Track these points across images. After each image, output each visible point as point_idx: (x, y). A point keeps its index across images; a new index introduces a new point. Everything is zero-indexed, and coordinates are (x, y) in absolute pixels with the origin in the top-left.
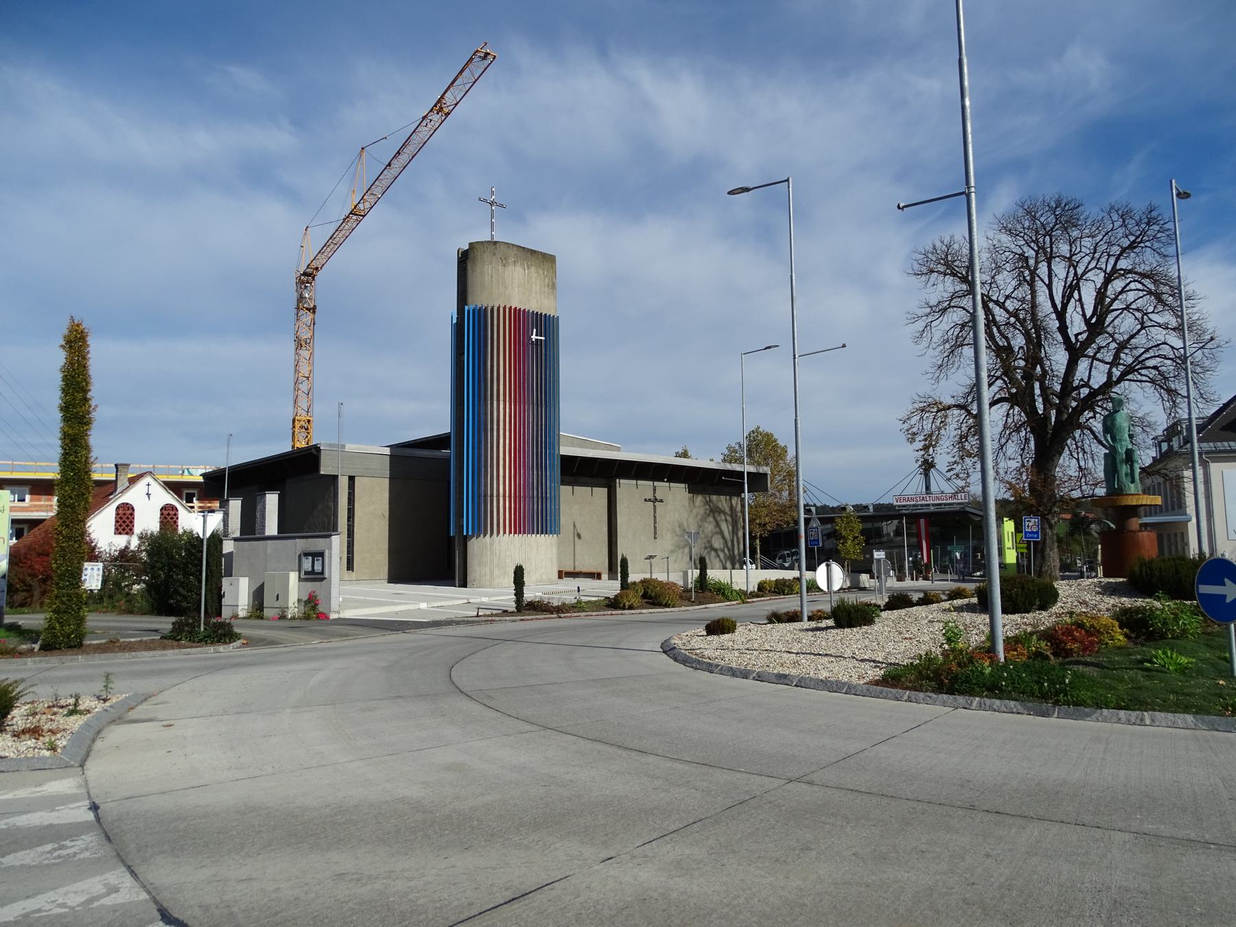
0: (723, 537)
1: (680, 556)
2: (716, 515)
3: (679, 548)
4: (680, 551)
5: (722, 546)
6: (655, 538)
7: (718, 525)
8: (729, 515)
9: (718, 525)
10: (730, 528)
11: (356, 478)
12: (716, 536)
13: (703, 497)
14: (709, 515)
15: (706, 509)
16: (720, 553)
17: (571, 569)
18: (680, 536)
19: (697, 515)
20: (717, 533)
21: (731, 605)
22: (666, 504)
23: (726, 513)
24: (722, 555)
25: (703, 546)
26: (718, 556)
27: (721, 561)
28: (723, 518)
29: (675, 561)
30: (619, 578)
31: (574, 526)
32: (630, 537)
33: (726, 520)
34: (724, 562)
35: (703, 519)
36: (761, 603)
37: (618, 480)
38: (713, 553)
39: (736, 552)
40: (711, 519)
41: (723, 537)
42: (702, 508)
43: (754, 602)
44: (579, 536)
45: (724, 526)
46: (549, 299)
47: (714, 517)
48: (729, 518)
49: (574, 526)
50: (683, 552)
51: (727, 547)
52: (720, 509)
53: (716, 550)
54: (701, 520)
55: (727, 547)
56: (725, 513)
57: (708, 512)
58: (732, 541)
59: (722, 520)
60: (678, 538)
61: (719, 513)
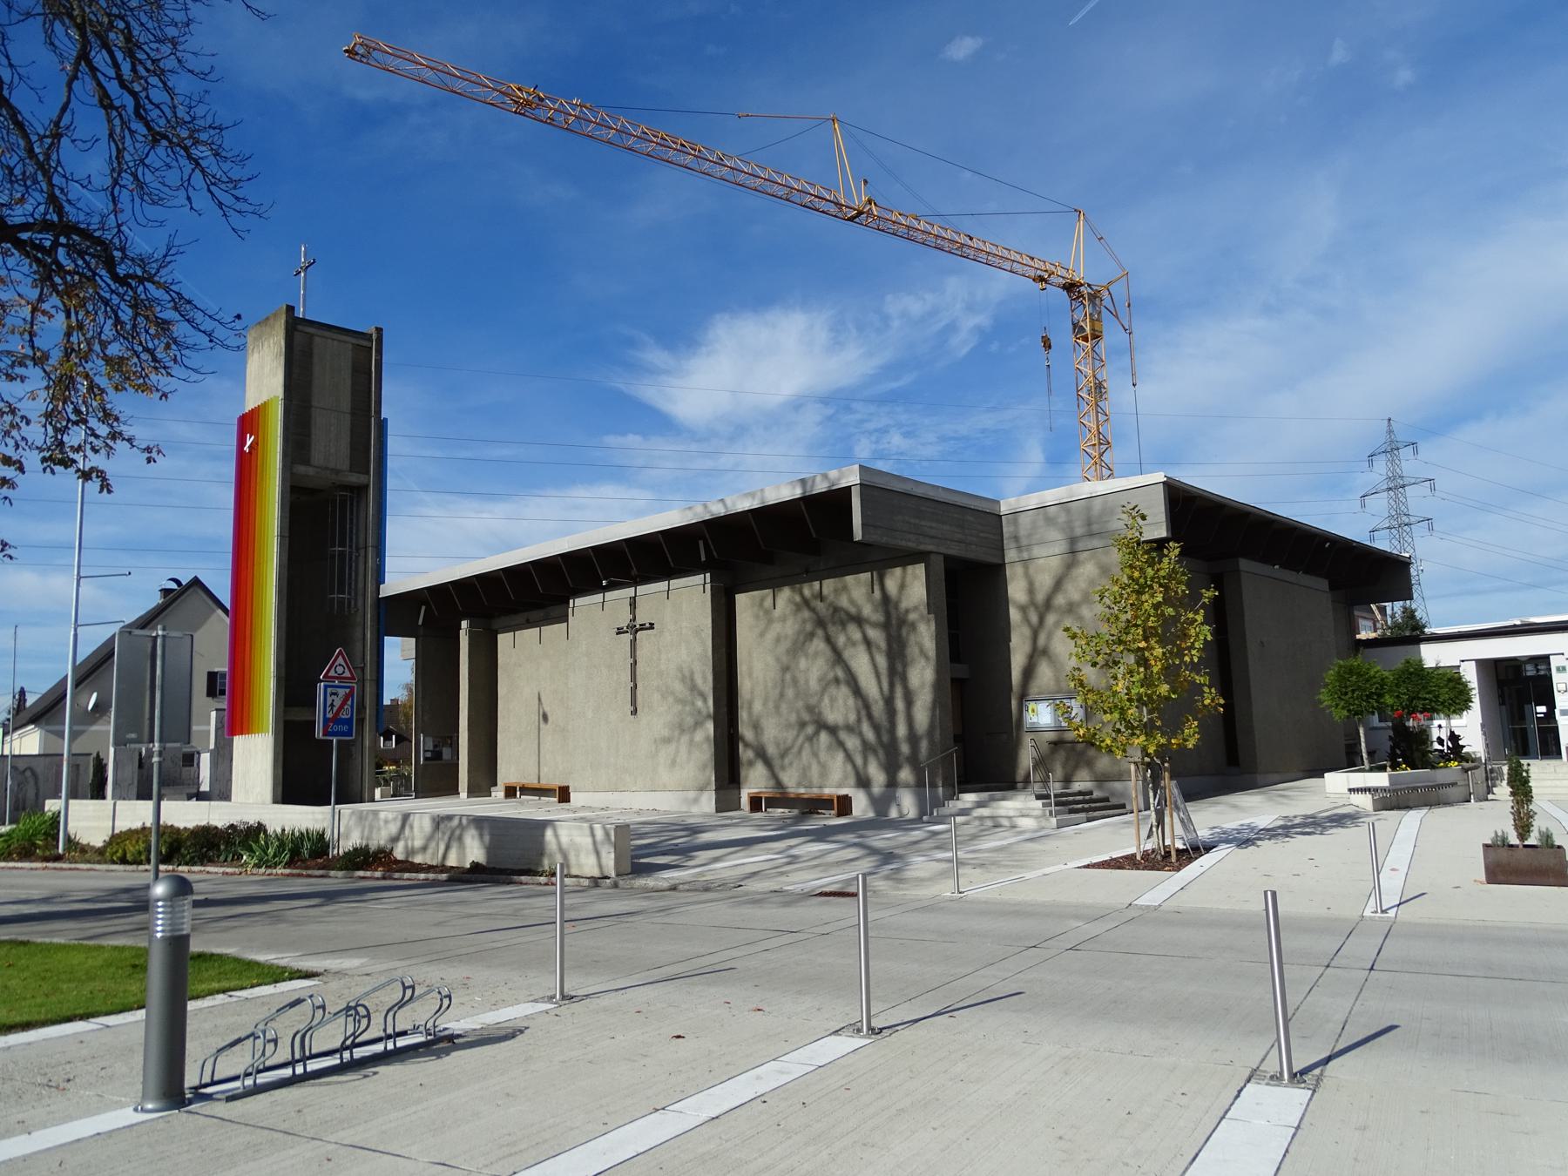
0: (857, 691)
1: (683, 749)
2: (832, 629)
3: (682, 731)
4: (685, 739)
5: (852, 718)
6: (634, 712)
7: (838, 658)
8: (875, 625)
9: (838, 658)
10: (882, 661)
11: (1551, 657)
12: (833, 690)
13: (793, 590)
14: (812, 635)
15: (804, 621)
16: (843, 735)
17: (531, 781)
18: (682, 702)
19: (778, 640)
20: (837, 681)
21: (70, 869)
22: (661, 632)
23: (867, 621)
24: (852, 743)
25: (793, 718)
26: (841, 744)
27: (849, 757)
28: (857, 636)
29: (674, 763)
30: (836, 809)
31: (539, 699)
32: (590, 714)
33: (868, 643)
34: (859, 761)
35: (798, 646)
36: (8, 872)
37: (571, 601)
38: (824, 737)
39: (902, 730)
40: (818, 644)
41: (857, 691)
42: (789, 623)
43: (78, 869)
44: (545, 718)
45: (861, 663)
46: (13, 326)
47: (829, 640)
48: (875, 634)
49: (539, 699)
50: (691, 741)
51: (870, 717)
52: (848, 613)
53: (833, 730)
54: (788, 652)
55: (870, 717)
56: (859, 620)
57: (809, 627)
58: (889, 702)
59: (854, 644)
60: (680, 707)
61: (843, 625)
